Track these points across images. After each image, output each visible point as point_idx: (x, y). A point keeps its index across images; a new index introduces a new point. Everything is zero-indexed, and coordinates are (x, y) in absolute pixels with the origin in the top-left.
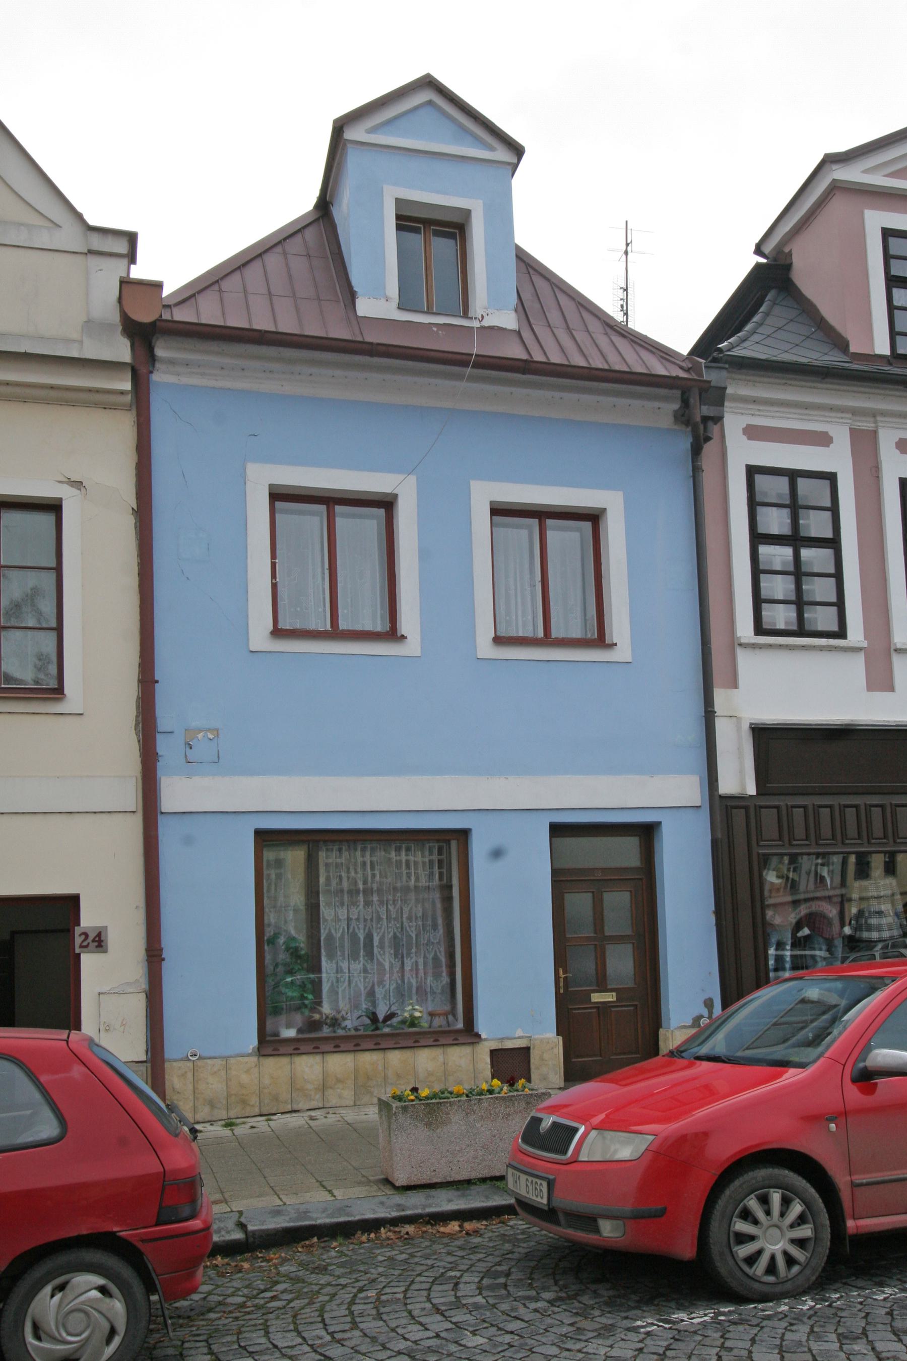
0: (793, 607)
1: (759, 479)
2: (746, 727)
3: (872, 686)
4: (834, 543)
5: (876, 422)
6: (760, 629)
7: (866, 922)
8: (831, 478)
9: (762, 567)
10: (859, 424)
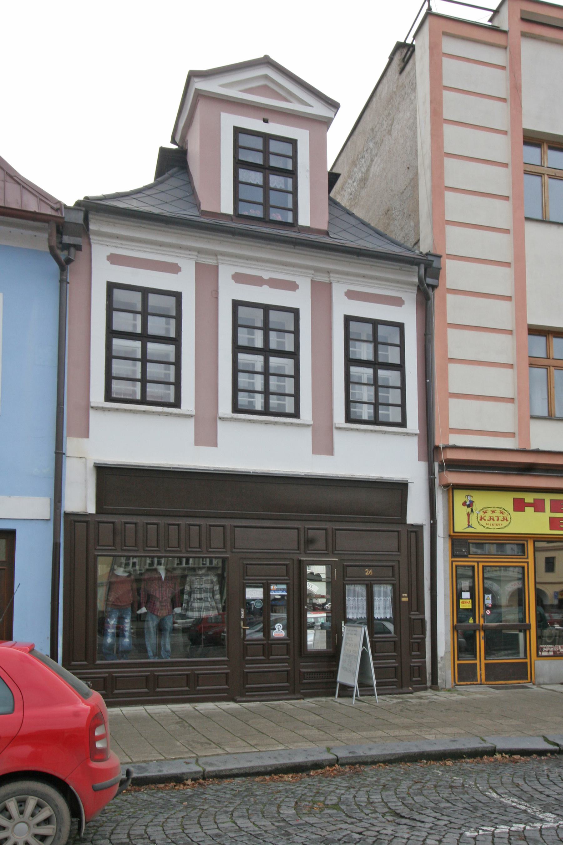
0: (372, 406)
1: (352, 324)
2: (91, 465)
3: (198, 442)
4: (400, 367)
5: (217, 259)
6: (348, 419)
7: (191, 604)
8: (401, 326)
9: (114, 354)
10: (204, 260)
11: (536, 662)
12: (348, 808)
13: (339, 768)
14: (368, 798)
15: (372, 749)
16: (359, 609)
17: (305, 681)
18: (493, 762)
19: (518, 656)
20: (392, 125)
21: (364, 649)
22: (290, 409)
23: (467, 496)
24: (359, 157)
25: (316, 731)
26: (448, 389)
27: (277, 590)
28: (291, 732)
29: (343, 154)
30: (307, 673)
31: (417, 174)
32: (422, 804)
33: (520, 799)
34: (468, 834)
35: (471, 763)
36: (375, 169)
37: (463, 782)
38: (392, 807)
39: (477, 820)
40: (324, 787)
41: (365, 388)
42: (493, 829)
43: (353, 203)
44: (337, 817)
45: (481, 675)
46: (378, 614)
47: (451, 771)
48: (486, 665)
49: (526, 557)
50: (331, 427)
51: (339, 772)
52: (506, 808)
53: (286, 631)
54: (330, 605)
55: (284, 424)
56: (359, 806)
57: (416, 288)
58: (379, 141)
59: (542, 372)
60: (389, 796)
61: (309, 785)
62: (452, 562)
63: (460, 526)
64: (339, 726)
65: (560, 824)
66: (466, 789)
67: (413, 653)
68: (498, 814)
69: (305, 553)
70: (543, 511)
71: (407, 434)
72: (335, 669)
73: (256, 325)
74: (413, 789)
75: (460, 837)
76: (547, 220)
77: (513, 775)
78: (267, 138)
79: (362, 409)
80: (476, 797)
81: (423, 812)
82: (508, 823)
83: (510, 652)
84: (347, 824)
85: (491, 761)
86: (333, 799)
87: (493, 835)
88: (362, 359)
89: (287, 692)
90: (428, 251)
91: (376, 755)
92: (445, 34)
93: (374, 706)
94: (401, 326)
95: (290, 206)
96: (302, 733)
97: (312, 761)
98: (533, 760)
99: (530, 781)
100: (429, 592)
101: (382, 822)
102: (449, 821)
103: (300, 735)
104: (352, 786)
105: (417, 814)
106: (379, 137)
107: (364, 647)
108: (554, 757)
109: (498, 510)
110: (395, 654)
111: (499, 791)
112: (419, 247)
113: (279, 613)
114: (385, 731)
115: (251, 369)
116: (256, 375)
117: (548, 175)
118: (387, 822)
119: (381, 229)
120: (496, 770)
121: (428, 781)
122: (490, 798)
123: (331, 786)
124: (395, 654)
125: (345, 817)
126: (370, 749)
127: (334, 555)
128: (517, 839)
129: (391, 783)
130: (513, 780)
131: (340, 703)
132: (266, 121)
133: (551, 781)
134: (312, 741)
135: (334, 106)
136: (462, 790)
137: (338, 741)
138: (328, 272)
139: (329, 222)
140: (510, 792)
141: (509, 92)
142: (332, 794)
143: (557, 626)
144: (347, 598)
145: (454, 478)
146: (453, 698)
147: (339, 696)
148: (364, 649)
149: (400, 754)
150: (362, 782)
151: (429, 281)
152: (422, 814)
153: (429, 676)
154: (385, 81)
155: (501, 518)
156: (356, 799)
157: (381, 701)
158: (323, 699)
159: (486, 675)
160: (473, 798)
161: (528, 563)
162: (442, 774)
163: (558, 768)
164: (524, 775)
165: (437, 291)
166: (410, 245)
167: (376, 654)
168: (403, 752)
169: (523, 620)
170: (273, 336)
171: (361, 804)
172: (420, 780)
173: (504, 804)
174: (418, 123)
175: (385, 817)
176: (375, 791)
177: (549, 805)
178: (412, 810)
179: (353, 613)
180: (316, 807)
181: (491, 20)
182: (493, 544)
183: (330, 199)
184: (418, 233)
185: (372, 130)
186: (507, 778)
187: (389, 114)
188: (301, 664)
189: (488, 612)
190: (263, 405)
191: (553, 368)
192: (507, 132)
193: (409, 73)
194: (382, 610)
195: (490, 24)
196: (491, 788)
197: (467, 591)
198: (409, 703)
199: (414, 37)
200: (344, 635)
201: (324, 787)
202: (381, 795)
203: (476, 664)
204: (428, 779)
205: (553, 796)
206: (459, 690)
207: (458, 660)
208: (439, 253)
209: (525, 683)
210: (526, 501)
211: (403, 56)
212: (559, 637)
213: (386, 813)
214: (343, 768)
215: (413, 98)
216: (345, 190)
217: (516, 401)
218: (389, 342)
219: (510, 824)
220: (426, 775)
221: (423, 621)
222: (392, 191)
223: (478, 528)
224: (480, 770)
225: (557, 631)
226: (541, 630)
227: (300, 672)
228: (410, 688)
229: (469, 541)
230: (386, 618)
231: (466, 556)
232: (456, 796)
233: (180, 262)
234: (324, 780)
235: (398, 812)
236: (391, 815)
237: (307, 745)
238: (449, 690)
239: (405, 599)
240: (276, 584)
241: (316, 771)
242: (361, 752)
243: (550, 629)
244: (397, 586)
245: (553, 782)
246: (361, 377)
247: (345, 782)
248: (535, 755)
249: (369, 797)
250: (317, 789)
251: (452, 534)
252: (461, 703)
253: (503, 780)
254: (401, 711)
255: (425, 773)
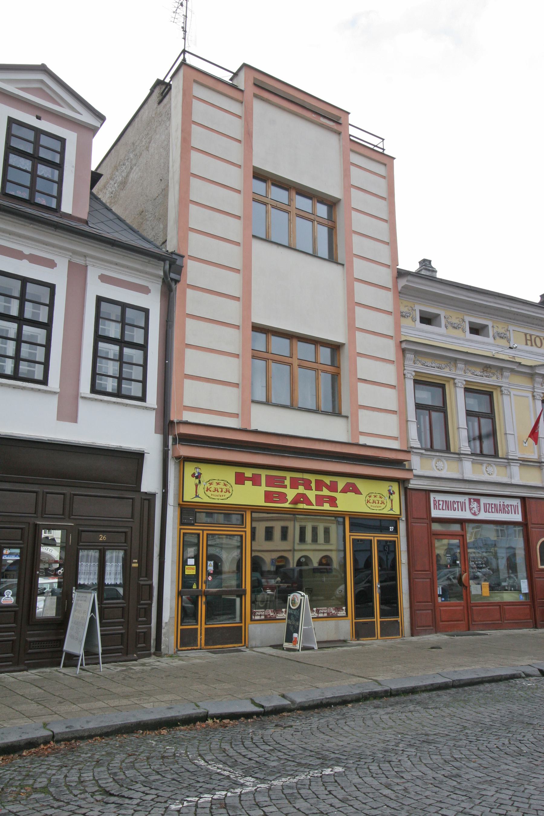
0: (116, 380)
1: (103, 304)
3: (61, 417)
4: (144, 347)
6: (94, 390)
8: (146, 311)
11: (250, 625)
12: (57, 790)
13: (54, 746)
14: (79, 778)
15: (90, 722)
16: (90, 574)
17: (30, 651)
18: (205, 728)
19: (235, 621)
20: (150, 143)
21: (92, 615)
22: (39, 376)
23: (196, 468)
24: (121, 163)
25: (36, 705)
26: (184, 371)
27: (10, 554)
28: (8, 708)
29: (108, 159)
30: (33, 642)
31: (167, 186)
32: (133, 779)
33: (225, 765)
34: (173, 807)
35: (185, 730)
36: (133, 176)
37: (175, 751)
38: (102, 785)
39: (184, 791)
40: (35, 768)
41: (111, 363)
42: (197, 799)
43: (113, 201)
44: (44, 802)
45: (201, 639)
46: (109, 580)
47: (165, 740)
48: (206, 629)
49: (244, 526)
50: (76, 396)
51: (53, 750)
52: (211, 775)
53: (15, 598)
54: (62, 570)
55: (32, 389)
56: (68, 786)
57: (161, 280)
58: (138, 154)
59: (261, 364)
60: (102, 773)
61: (20, 767)
62: (180, 529)
63: (189, 496)
64: (60, 699)
65: (258, 788)
66: (176, 758)
67: (140, 619)
68: (204, 782)
69: (42, 517)
70: (260, 485)
71: (146, 408)
72: (62, 637)
73: (111, 318)
74: (126, 763)
75: (165, 811)
76: (269, 240)
77: (222, 740)
78: (38, 132)
79: (107, 382)
80: (184, 766)
81: (132, 787)
82: (211, 791)
83: (230, 616)
84: (53, 809)
85: (203, 727)
86: (42, 781)
87: (196, 806)
88: (110, 336)
89: (11, 663)
90: (173, 251)
91: (93, 728)
92: (195, 81)
93: (98, 676)
94: (146, 311)
95: (55, 193)
96: (19, 708)
97: (26, 739)
98: (241, 723)
99: (236, 745)
100: (158, 558)
101: (90, 803)
102: (156, 795)
103: (17, 711)
104: (65, 765)
105: (127, 790)
106: (139, 150)
107: (92, 614)
108: (259, 719)
109: (222, 482)
110: (122, 620)
111: (207, 758)
112: (166, 246)
113: (10, 578)
114: (105, 701)
115: (4, 335)
116: (8, 341)
117: (271, 205)
118: (95, 802)
119: (135, 226)
120: (207, 736)
121: (142, 752)
122: (198, 766)
123: (43, 766)
124: (122, 620)
125: (52, 801)
126: (88, 722)
127: (70, 519)
128: (219, 808)
129: (105, 758)
130: (220, 745)
131: (64, 674)
132: (39, 118)
133: (254, 743)
134: (29, 717)
135: (102, 118)
136: (173, 760)
137: (56, 716)
138: (85, 256)
139: (89, 213)
140: (217, 758)
141: (243, 136)
142: (43, 775)
143: (269, 592)
144: (80, 563)
145: (185, 451)
146: (174, 664)
147: (64, 666)
148: (92, 615)
149: (117, 725)
150: (75, 759)
151: (173, 275)
152: (131, 789)
153: (154, 642)
154: (146, 107)
155: (224, 490)
156: (67, 779)
157: (105, 669)
158: (48, 670)
159: (205, 639)
160: (182, 767)
161: (245, 532)
162: (156, 745)
163: (261, 730)
164: (231, 740)
165: (179, 286)
166: (158, 243)
167: (104, 621)
168: (120, 723)
169: (239, 585)
170: (28, 306)
171: (71, 784)
172: (134, 753)
173: (210, 771)
174: (171, 145)
175: (94, 797)
176: (87, 768)
177: (250, 769)
178: (122, 786)
179: (85, 579)
180: (23, 793)
181: (231, 79)
182: (221, 513)
183: (92, 194)
184: (166, 235)
185: (133, 144)
186: (216, 743)
187: (148, 134)
188: (28, 632)
189: (210, 578)
190: (13, 370)
191: (271, 361)
192: (240, 166)
193: (166, 105)
194: (113, 576)
195: (231, 82)
196: (200, 755)
197: (192, 558)
198: (132, 671)
199: (172, 78)
200: (74, 602)
201: (35, 768)
202: (93, 772)
203: (197, 629)
204: (142, 750)
205: (254, 759)
206: (181, 655)
207: (181, 625)
208: (182, 253)
209: (239, 647)
210: (246, 475)
211: (162, 91)
212: (270, 601)
213: (96, 792)
214: (59, 745)
215: (168, 125)
216: (107, 189)
217: (240, 386)
218: (135, 324)
219: (213, 792)
220: (141, 746)
221: (151, 586)
222: (147, 196)
223: (204, 499)
224: (192, 737)
225: (269, 596)
226: (255, 595)
227: (26, 640)
228: (135, 655)
229: (196, 510)
230: (116, 583)
231: (193, 525)
232: (166, 767)
233: (57, 259)
234: (36, 761)
235: (107, 789)
236: (100, 794)
237: (22, 722)
238: (171, 656)
239: (135, 565)
240: (10, 548)
241: (30, 750)
242: (77, 726)
243: (263, 594)
244: (129, 552)
245: (256, 745)
246: (108, 352)
247: (58, 761)
248: (242, 718)
249: (80, 775)
250: (27, 771)
251: (181, 503)
252: (180, 668)
253: (211, 746)
254: (124, 679)
255: (139, 744)
